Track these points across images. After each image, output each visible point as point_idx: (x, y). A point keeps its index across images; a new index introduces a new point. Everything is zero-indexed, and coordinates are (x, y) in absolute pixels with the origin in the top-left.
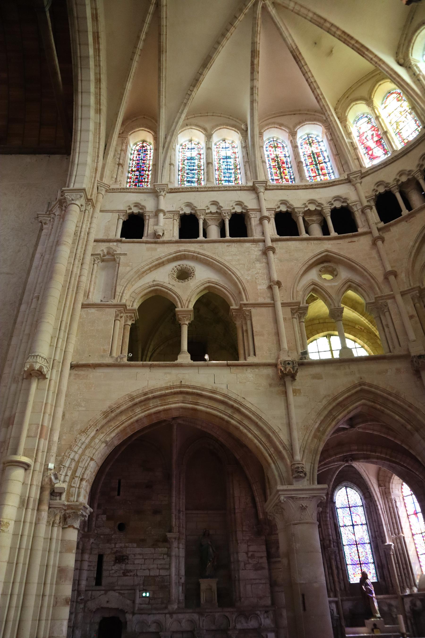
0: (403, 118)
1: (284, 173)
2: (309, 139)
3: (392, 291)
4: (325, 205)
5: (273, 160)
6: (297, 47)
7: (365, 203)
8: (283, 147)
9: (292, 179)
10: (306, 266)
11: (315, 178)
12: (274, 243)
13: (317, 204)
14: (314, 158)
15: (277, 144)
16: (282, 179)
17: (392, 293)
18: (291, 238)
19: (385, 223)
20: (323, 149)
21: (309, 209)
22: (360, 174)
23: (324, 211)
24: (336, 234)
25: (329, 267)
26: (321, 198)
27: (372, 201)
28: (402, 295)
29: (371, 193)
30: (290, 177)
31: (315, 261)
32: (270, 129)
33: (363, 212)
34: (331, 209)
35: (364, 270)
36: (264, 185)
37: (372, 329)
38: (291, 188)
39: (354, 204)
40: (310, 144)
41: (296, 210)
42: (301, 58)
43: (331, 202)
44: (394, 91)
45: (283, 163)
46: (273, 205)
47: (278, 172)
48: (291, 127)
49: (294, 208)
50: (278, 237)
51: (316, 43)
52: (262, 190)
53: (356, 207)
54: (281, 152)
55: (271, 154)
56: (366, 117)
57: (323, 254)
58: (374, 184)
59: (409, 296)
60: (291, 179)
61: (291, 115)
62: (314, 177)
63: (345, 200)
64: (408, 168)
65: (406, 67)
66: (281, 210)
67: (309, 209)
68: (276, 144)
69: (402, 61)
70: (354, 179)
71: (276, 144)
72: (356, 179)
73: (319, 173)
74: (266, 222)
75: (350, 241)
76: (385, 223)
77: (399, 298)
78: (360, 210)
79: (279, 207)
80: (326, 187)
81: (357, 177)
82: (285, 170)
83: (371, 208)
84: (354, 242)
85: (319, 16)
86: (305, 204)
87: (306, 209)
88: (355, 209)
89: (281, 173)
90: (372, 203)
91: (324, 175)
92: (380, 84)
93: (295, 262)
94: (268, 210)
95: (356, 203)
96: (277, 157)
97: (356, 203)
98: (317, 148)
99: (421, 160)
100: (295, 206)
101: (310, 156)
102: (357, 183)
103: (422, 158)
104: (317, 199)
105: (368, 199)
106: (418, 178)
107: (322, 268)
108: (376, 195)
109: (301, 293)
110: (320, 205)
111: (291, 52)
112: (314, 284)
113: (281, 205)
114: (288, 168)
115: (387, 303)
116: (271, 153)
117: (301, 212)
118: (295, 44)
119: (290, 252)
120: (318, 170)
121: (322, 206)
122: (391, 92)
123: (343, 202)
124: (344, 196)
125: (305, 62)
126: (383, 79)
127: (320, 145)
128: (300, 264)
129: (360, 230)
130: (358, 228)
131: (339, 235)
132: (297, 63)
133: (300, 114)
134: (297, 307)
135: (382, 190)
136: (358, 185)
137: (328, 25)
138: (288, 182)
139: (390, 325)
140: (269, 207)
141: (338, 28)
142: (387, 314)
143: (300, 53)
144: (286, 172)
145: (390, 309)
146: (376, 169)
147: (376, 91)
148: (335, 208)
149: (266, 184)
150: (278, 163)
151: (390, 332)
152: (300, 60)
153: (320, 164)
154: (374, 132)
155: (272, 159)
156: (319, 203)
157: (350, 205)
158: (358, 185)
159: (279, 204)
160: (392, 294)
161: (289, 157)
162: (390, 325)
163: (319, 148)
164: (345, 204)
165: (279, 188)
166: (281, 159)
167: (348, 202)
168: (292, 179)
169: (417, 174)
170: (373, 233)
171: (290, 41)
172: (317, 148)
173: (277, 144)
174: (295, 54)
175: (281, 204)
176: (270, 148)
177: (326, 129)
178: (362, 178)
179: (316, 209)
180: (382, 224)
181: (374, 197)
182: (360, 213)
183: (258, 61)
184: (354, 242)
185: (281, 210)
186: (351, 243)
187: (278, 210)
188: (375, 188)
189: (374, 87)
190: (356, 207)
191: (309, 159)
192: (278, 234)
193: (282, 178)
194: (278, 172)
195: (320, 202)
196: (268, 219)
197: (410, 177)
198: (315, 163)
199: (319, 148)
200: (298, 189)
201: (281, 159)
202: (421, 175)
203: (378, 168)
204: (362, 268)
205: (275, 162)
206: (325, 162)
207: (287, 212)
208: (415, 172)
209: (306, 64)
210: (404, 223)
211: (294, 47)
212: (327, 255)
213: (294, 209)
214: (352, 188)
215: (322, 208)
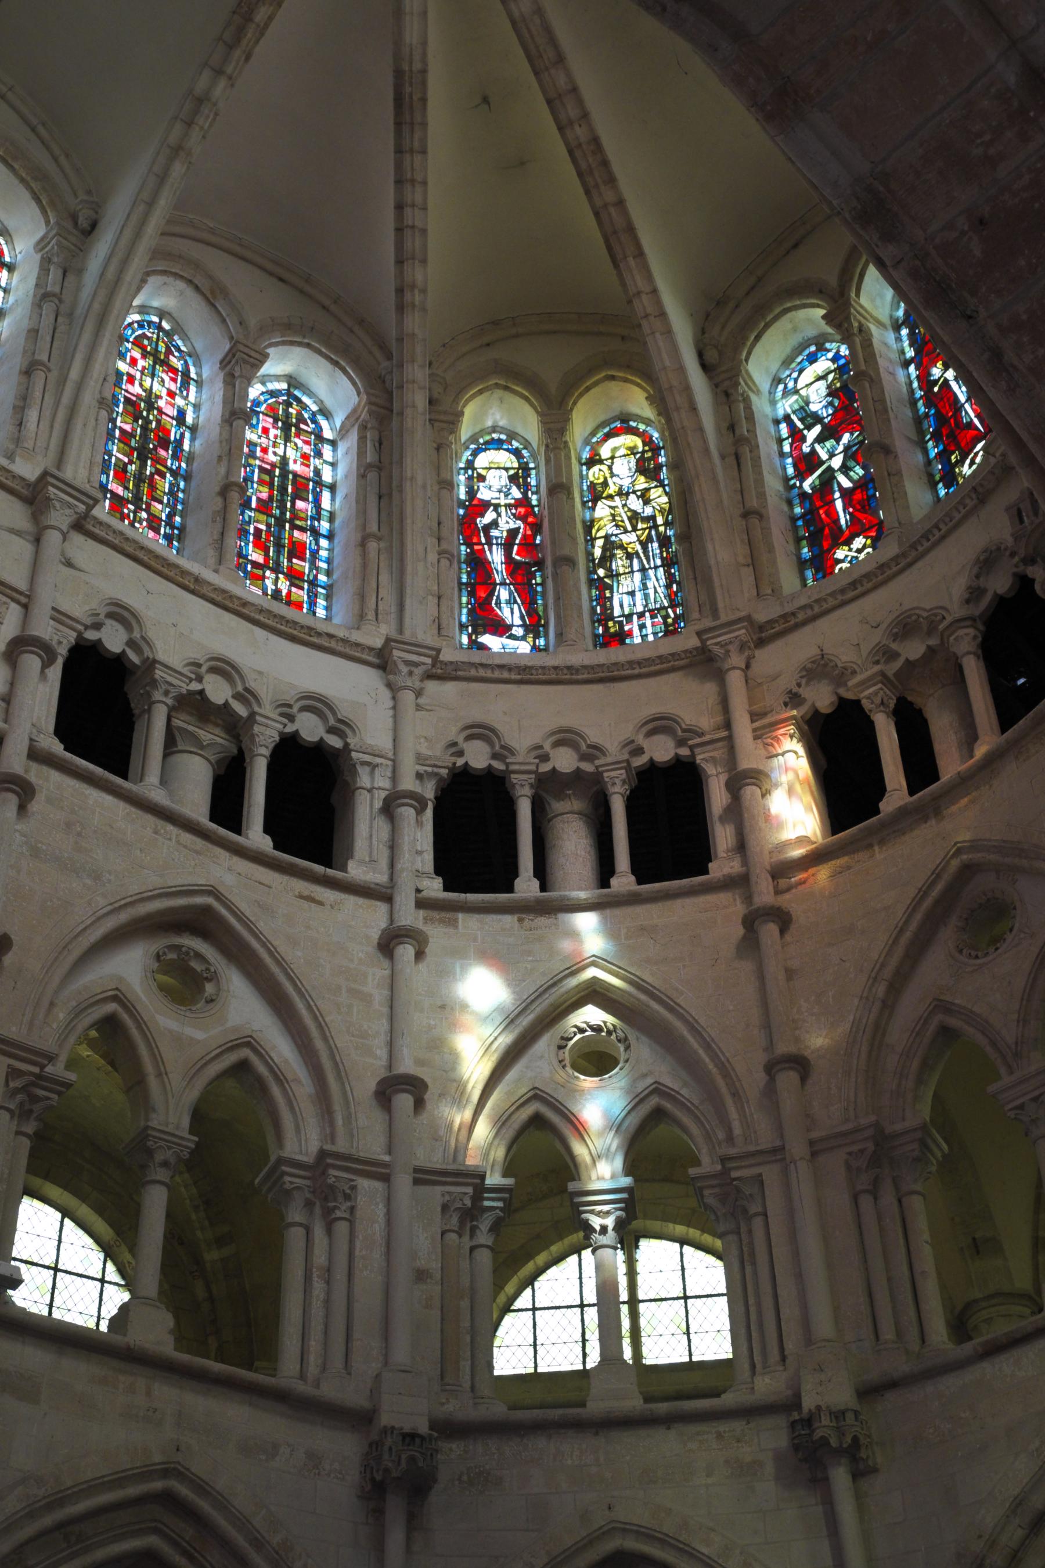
0: (629, 539)
1: (153, 487)
2: (288, 404)
3: (390, 1152)
4: (267, 709)
5: (130, 408)
6: (424, 71)
7: (408, 783)
8: (186, 374)
9: (173, 527)
10: (123, 917)
11: (259, 572)
12: (34, 766)
13: (240, 688)
14: (283, 490)
15: (169, 352)
16: (138, 509)
17: (387, 1158)
18: (107, 781)
19: (446, 889)
20: (327, 476)
21: (202, 692)
22: (429, 661)
23: (256, 729)
24: (264, 843)
25: (199, 956)
26: (260, 673)
27: (433, 782)
28: (416, 1182)
29: (437, 751)
30: (170, 516)
31: (161, 913)
32: (170, 280)
33: (388, 809)
34: (281, 734)
35: (320, 1027)
36: (82, 507)
37: (199, 1234)
38: (172, 574)
39: (367, 758)
40: (286, 429)
41: (159, 673)
42: (418, 118)
43: (290, 706)
44: (642, 427)
45: (165, 444)
46: (78, 608)
47: (132, 468)
48: (253, 322)
49: (155, 661)
50: (57, 747)
51: (485, 100)
52: (60, 517)
53: (372, 773)
54: (171, 394)
55: (131, 380)
56: (517, 453)
57: (199, 900)
58: (460, 725)
59: (436, 1194)
60: (170, 523)
61: (271, 274)
62: (255, 564)
63: (341, 727)
64: (594, 736)
65: (717, 386)
66: (99, 641)
67: (202, 692)
68: (162, 347)
69: (712, 356)
70: (404, 669)
71: (162, 347)
72: (411, 673)
73: (278, 563)
74: (32, 662)
75: (306, 893)
76: (446, 889)
77: (403, 1182)
78: (383, 794)
79: (97, 626)
80: (293, 639)
81: (416, 665)
82: (163, 476)
83: (420, 811)
84: (320, 903)
85: (548, 30)
86: (199, 666)
87: (195, 686)
88: (364, 779)
89: (139, 478)
90: (429, 791)
91: (295, 577)
92: (613, 378)
93: (89, 882)
94: (59, 616)
95: (379, 760)
96: (151, 406)
97: (379, 760)
98: (305, 457)
99: (644, 730)
100: (161, 656)
101: (270, 473)
102: (405, 688)
103: (650, 726)
104: (245, 671)
105: (422, 769)
106: (612, 790)
107: (168, 947)
108: (453, 769)
109: (61, 1016)
110: (247, 696)
111: (398, 74)
112: (118, 998)
113: (109, 622)
114: (175, 473)
115: (353, 1188)
116: (132, 371)
117: (174, 692)
118: (424, 54)
119: (79, 834)
120: (279, 546)
121: (256, 709)
122: (633, 424)
123: (331, 730)
124: (344, 712)
125: (424, 140)
126: (628, 367)
127: (319, 454)
128: (102, 902)
129: (356, 871)
130: (352, 857)
131: (276, 853)
132: (398, 124)
133: (302, 292)
134: (36, 1070)
135: (478, 757)
136: (408, 697)
137: (562, 81)
138: (157, 531)
139: (340, 1275)
140: (65, 606)
141: (585, 116)
142: (342, 1227)
143: (424, 100)
144: (164, 485)
145: (358, 1213)
146: (489, 674)
147: (588, 389)
148: (295, 735)
149: (90, 508)
150: (145, 428)
151: (327, 1302)
152: (412, 124)
153: (294, 527)
154: (519, 523)
155: (127, 400)
156: (246, 689)
157: (354, 754)
158: (408, 697)
159: (103, 611)
160: (385, 1165)
161: (193, 429)
162: (340, 1275)
163: (315, 462)
164: (335, 742)
165: (129, 549)
166: (158, 422)
167: (352, 741)
168: (173, 527)
169: (613, 774)
170: (397, 906)
171: (411, 35)
172: (305, 457)
173: (169, 352)
174: (408, 90)
175: (110, 615)
176: (137, 354)
177: (370, 413)
178: (429, 676)
179: (226, 704)
180: (434, 887)
181: (444, 772)
182: (378, 804)
183: (271, 18)
184: (320, 903)
185: (100, 641)
186: (305, 904)
187: (91, 635)
188: (460, 739)
189: (591, 371)
190: (372, 773)
191: (261, 482)
192: (61, 732)
193: (137, 500)
194: (132, 468)
195: (252, 685)
196: (48, 654)
197: (588, 767)
198: (277, 512)
199: (315, 462)
200: (192, 592)
201: (158, 422)
202: (624, 782)
203: (497, 674)
204: (315, 1018)
205: (136, 420)
206: (316, 533)
207: (119, 660)
208: (609, 760)
209: (424, 152)
210: (509, 920)
211: (417, 66)
212: (207, 910)
213: (151, 664)
214: (385, 694)
215: (252, 715)
